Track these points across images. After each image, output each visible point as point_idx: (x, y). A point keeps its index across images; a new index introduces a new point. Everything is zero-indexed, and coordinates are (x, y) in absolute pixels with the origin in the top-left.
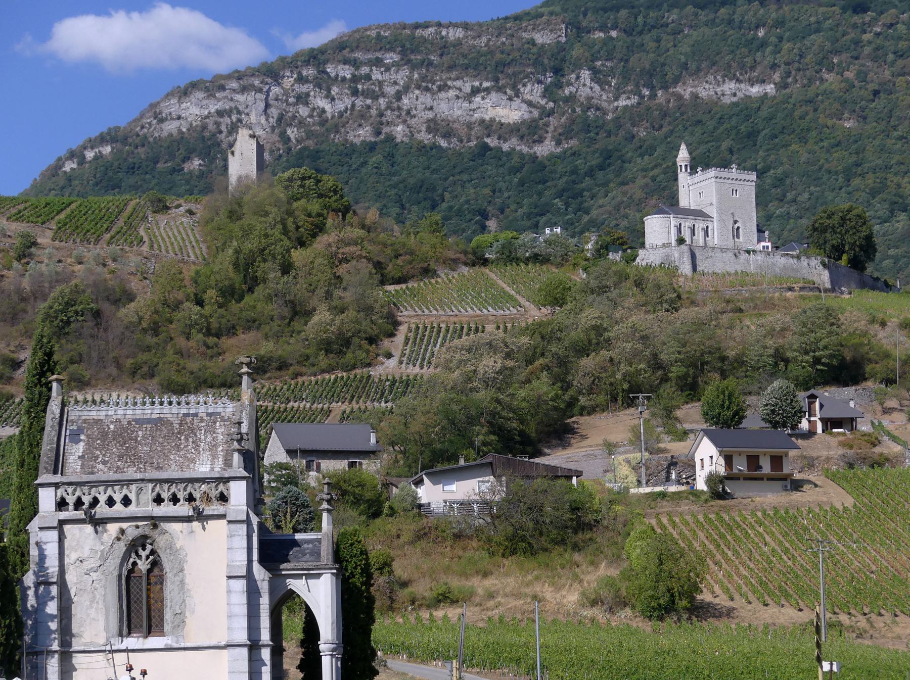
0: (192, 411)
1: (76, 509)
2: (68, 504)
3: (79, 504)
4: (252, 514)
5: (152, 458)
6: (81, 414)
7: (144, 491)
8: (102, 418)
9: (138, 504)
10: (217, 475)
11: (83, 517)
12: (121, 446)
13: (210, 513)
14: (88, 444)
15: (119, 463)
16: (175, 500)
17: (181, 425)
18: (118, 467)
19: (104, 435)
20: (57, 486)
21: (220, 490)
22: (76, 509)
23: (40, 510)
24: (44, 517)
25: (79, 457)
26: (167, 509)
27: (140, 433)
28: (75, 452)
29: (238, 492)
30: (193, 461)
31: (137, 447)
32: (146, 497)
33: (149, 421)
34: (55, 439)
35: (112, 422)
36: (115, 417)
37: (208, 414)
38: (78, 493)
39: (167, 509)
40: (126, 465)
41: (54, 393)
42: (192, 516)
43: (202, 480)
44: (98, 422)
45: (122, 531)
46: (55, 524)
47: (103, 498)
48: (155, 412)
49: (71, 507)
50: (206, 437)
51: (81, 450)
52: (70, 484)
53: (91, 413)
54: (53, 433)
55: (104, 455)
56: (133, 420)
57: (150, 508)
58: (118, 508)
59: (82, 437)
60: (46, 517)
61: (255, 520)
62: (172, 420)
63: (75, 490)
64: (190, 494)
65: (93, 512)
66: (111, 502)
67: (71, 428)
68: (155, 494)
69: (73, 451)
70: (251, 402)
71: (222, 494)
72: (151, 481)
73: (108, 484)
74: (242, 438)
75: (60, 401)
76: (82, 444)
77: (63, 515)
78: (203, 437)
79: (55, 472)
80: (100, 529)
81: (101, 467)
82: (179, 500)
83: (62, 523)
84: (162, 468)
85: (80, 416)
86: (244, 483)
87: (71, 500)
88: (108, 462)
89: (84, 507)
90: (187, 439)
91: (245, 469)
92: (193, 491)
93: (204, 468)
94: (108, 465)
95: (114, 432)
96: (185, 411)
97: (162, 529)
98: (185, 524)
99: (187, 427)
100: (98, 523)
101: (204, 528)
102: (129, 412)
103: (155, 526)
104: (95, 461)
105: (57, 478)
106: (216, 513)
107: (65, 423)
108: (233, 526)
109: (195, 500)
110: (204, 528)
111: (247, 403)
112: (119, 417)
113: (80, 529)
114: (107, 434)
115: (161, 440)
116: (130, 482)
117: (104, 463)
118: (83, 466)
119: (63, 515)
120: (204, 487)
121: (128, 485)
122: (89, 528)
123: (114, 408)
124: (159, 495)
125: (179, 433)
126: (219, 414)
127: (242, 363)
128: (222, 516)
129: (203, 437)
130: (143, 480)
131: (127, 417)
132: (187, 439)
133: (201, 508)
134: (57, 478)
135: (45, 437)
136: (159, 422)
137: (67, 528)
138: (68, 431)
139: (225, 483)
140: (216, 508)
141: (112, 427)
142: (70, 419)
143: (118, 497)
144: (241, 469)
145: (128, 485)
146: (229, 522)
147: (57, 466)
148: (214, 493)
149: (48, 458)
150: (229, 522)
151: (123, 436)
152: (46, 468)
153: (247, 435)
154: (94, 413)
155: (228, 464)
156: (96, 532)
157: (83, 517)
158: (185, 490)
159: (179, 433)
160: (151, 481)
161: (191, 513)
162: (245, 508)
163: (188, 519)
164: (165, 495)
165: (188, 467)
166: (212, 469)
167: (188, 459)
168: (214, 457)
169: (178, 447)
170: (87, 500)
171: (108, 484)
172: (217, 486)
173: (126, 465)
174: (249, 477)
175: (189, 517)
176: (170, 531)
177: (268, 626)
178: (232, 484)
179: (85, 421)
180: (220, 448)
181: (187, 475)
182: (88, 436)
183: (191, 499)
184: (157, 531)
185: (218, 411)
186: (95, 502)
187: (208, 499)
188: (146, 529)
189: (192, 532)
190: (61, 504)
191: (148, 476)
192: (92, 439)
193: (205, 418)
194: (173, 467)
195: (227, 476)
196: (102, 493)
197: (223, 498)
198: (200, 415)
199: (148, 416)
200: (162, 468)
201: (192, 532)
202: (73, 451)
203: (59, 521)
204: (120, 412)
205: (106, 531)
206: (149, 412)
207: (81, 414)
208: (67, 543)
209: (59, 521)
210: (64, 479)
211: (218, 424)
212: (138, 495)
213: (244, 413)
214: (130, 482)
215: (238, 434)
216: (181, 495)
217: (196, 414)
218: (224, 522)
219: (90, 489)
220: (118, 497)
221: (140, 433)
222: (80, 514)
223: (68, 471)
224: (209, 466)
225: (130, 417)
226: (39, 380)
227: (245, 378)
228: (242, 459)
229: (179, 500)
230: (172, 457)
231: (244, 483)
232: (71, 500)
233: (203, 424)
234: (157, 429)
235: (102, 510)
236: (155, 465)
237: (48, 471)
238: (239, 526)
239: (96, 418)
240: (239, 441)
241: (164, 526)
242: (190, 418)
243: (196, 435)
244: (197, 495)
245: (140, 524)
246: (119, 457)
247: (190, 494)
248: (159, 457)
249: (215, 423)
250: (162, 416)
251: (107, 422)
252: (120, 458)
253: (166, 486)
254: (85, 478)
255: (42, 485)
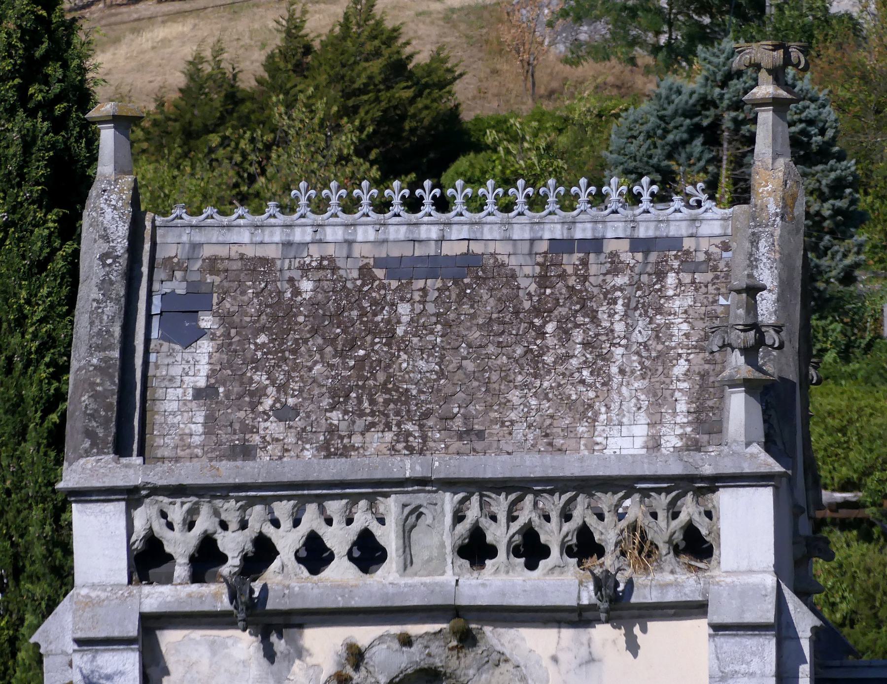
0: (583, 232)
1: (198, 575)
2: (170, 558)
3: (206, 559)
4: (793, 602)
5: (447, 399)
6: (198, 237)
7: (427, 519)
8: (272, 252)
9: (408, 563)
10: (676, 469)
11: (224, 603)
12: (341, 354)
13: (653, 597)
14: (225, 346)
15: (335, 416)
16: (531, 550)
17: (543, 280)
18: (332, 430)
19: (281, 314)
20: (132, 497)
21: (683, 518)
22: (198, 575)
23: (78, 578)
24: (89, 603)
25: (199, 394)
26: (501, 581)
27: (404, 309)
28: (184, 373)
29: (747, 526)
30: (586, 412)
31: (394, 358)
32: (433, 540)
33: (433, 266)
34: (117, 330)
35: (305, 270)
36: (315, 251)
37: (638, 245)
38: (204, 523)
39: (501, 581)
40: (360, 423)
41: (105, 167)
42: (592, 607)
43: (625, 485)
44: (257, 267)
45: (356, 656)
46: (132, 629)
47: (288, 542)
48: (456, 233)
49: (181, 570)
50: (630, 328)
51: (204, 369)
52: (178, 491)
53: (234, 236)
54: (111, 309)
55: (282, 388)
56: (379, 262)
57: (449, 577)
58: (341, 571)
59: (206, 321)
60: (100, 602)
61: (804, 622)
62: (513, 262)
63: (193, 512)
64: (584, 532)
65: (257, 586)
66: (315, 555)
67: (167, 288)
68: (463, 528)
69: (176, 371)
70: (788, 203)
71: (690, 531)
72: (450, 484)
73: (305, 492)
74: (760, 341)
75: (127, 195)
76: (205, 346)
77: (156, 597)
78: (619, 327)
79: (121, 449)
80: (280, 645)
81: (274, 427)
82: (545, 552)
83: (152, 624)
84: (480, 435)
85: (195, 246)
86: (765, 496)
87: (180, 545)
88: (295, 410)
89: (225, 570)
90: (564, 334)
91: (769, 446)
92: (592, 522)
93: (624, 441)
94: (298, 423)
95: (314, 304)
96: (558, 232)
97: (490, 650)
98: (567, 633)
99: (565, 289)
100: (274, 625)
101: (633, 647)
102: (365, 234)
103: (467, 639)
104: (253, 406)
105: (130, 472)
106: (671, 596)
107: (145, 270)
108: (730, 644)
109: (600, 551)
110: (633, 647)
111: (773, 207)
112: (330, 250)
113: (213, 645)
114: (290, 312)
115: (475, 335)
116: (377, 488)
117: (284, 414)
118: (211, 422)
119: (156, 597)
120: (633, 507)
121: (372, 499)
122: (243, 644)
123: (312, 218)
124: (477, 533)
125: (537, 311)
126: (675, 243)
127: (757, 67)
128: (695, 609)
129: (619, 327)
130: (423, 482)
131: (357, 251)
132: (564, 334)
133: (622, 578)
134: (130, 472)
135: (82, 318)
136: (468, 270)
137: (170, 639)
138: (157, 301)
139: (700, 493)
140: (669, 581)
141: (306, 286)
142: (160, 255)
143: (338, 538)
144: (756, 449)
145: (372, 499)
146: (718, 628)
147: (128, 431)
148: (663, 530)
149: (95, 396)
150: (718, 628)
151: (347, 316)
152: (90, 434)
153: (778, 329)
154: (244, 235)
155: (707, 424)
156: (270, 655)
157: (224, 603)
158: (566, 516)
159: (537, 311)
160: (450, 484)
161: (588, 596)
162: (770, 580)
163: (577, 617)
164: (499, 534)
165: (569, 430)
166: (654, 445)
167: (571, 405)
168: (659, 400)
169: (534, 359)
170: (233, 545)
171: (305, 492)
172: (673, 503)
173: (360, 423)
174: (779, 475)
175: (580, 610)
176: (517, 657)
177: (136, 355)
178: (727, 500)
179: (212, 264)
180: (681, 368)
181: (572, 465)
182: (225, 318)
183: (585, 547)
184: (471, 656)
185: (673, 231)
186: (262, 553)
187: (643, 549)
188: (436, 648)
189: (591, 660)
190: (148, 560)
191: (441, 464)
192: (240, 327)
193: (627, 258)
194: (520, 431)
195: (708, 470)
196: (286, 523)
197: (696, 547)
198: (609, 247)
199: (431, 250)
200: (480, 435)
201: (591, 660)
202: (176, 371)
203: (145, 618)
204: (334, 234)
205: (300, 653)
206: (434, 233)
207: (198, 237)
208: (116, 503)
209: (145, 618)
210: (158, 476)
211: (671, 279)
212: (406, 533)
213: (762, 244)
214: (377, 488)
215: (748, 328)
216: (552, 535)
217: (595, 244)
218: (699, 627)
219: (243, 509)
220: (338, 538)
221: (404, 309)
222: (214, 595)
223: (163, 442)
224: (641, 430)
225: (367, 250)
226: (22, 90)
227: (766, 117)
228: (757, 409)
229: (545, 552)
230: (515, 396)
231: (765, 496)
232: (180, 545)
233: (620, 280)
234: (462, 295)
235: (285, 582)
236: (458, 424)
237: (96, 446)
238: (750, 642)
239: (250, 252)
240: (750, 353)
241: (496, 637)
242: (576, 257)
243: (595, 320)
244: (607, 534)
245: (415, 630)
246: (333, 393)
247: (584, 532)
248: (472, 398)
249: (661, 275)
250: (477, 248)
251: (288, 267)
252: (339, 396)
253: (500, 504)
254: (229, 472)
255: (84, 495)
